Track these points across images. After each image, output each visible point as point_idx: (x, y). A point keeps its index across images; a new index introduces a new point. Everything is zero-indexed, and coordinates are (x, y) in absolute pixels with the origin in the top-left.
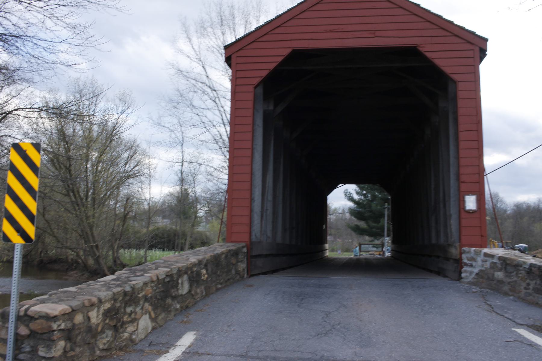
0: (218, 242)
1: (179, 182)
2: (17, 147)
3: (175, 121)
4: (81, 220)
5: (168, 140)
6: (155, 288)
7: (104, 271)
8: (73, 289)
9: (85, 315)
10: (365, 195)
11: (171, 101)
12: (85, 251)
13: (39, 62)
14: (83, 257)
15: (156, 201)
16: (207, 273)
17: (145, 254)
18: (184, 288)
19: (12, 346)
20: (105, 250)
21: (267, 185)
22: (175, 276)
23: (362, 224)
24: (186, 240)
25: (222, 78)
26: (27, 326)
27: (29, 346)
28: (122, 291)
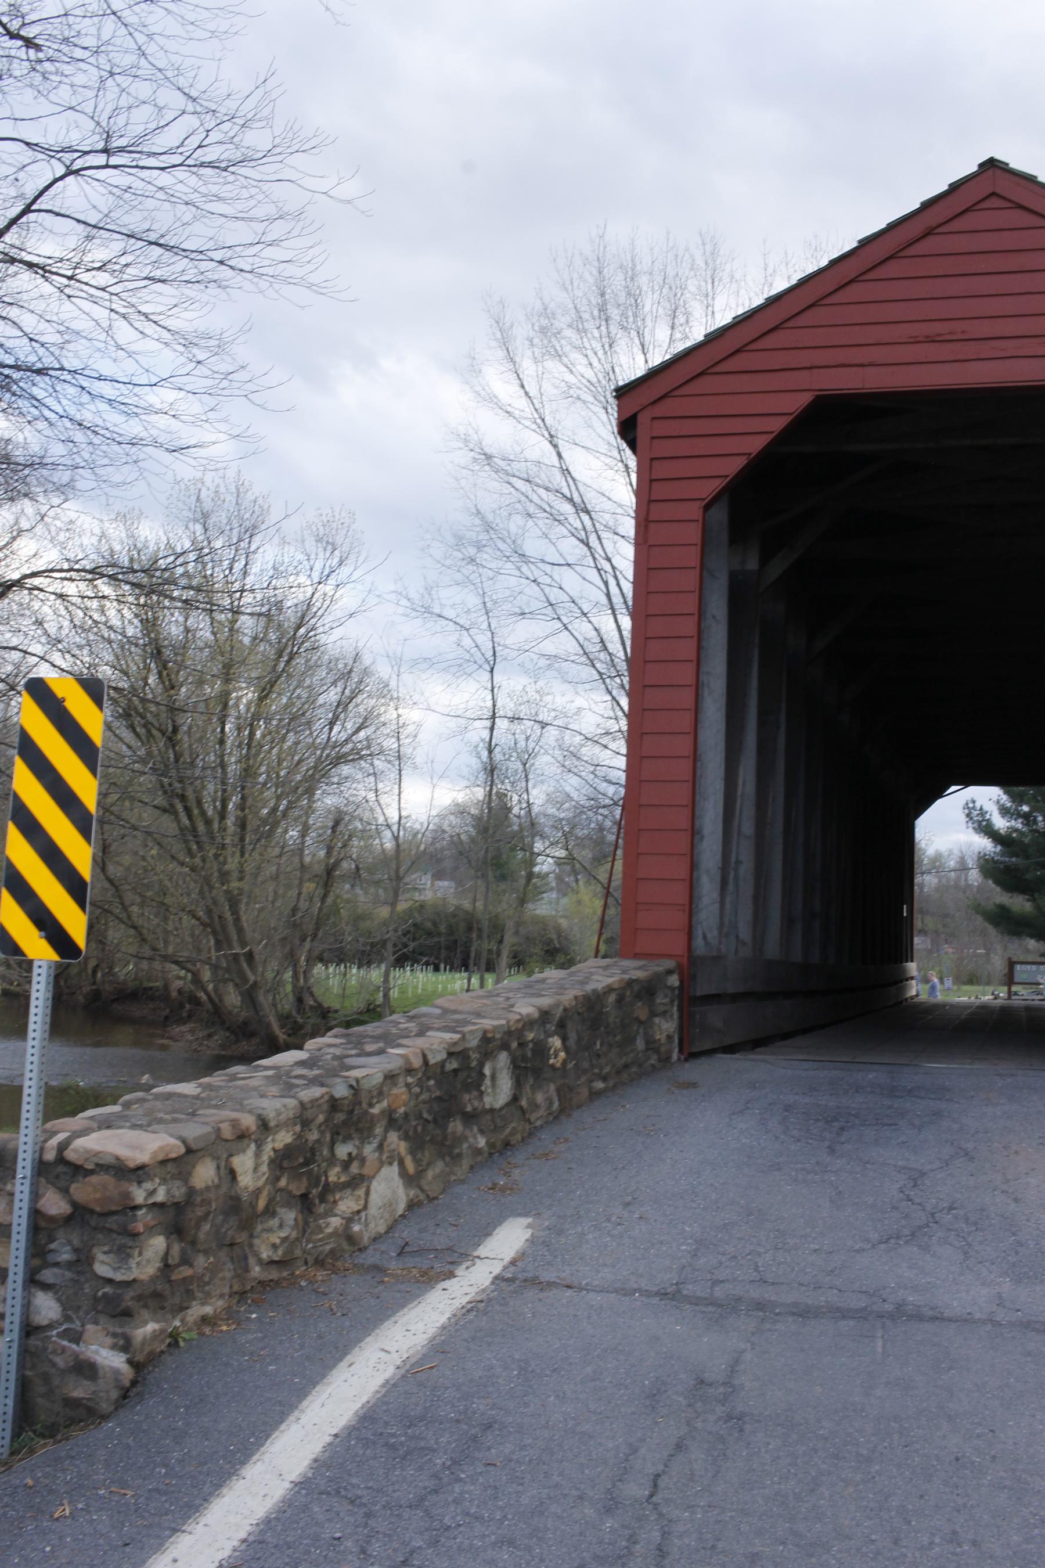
0: (596, 957)
1: (482, 776)
2: (39, 690)
3: (473, 601)
4: (207, 880)
5: (450, 656)
6: (417, 1090)
7: (268, 1025)
8: (187, 1088)
9: (223, 1164)
10: (1026, 817)
11: (460, 542)
12: (215, 968)
13: (96, 440)
14: (211, 987)
15: (417, 826)
16: (566, 1048)
17: (386, 980)
18: (499, 1089)
19: (22, 1245)
20: (274, 965)
21: (739, 793)
22: (474, 1055)
23: (1020, 904)
24: (501, 942)
25: (611, 480)
26: (65, 1191)
27: (68, 1248)
28: (326, 1098)
